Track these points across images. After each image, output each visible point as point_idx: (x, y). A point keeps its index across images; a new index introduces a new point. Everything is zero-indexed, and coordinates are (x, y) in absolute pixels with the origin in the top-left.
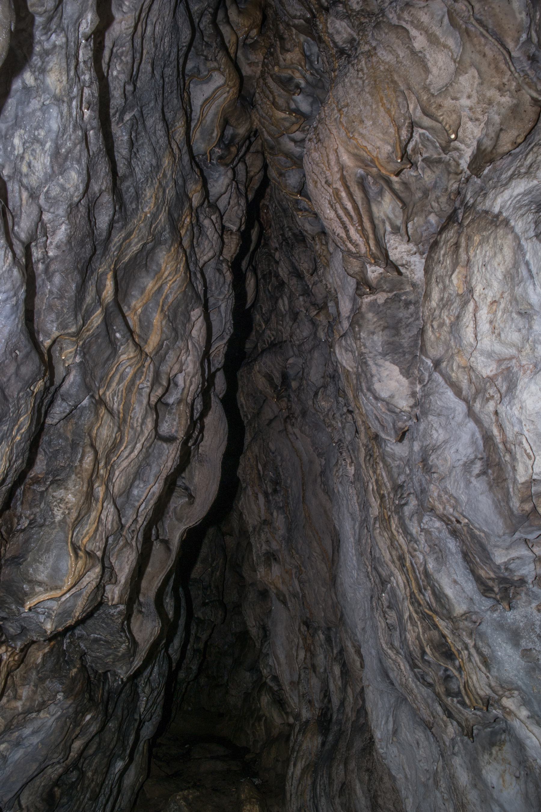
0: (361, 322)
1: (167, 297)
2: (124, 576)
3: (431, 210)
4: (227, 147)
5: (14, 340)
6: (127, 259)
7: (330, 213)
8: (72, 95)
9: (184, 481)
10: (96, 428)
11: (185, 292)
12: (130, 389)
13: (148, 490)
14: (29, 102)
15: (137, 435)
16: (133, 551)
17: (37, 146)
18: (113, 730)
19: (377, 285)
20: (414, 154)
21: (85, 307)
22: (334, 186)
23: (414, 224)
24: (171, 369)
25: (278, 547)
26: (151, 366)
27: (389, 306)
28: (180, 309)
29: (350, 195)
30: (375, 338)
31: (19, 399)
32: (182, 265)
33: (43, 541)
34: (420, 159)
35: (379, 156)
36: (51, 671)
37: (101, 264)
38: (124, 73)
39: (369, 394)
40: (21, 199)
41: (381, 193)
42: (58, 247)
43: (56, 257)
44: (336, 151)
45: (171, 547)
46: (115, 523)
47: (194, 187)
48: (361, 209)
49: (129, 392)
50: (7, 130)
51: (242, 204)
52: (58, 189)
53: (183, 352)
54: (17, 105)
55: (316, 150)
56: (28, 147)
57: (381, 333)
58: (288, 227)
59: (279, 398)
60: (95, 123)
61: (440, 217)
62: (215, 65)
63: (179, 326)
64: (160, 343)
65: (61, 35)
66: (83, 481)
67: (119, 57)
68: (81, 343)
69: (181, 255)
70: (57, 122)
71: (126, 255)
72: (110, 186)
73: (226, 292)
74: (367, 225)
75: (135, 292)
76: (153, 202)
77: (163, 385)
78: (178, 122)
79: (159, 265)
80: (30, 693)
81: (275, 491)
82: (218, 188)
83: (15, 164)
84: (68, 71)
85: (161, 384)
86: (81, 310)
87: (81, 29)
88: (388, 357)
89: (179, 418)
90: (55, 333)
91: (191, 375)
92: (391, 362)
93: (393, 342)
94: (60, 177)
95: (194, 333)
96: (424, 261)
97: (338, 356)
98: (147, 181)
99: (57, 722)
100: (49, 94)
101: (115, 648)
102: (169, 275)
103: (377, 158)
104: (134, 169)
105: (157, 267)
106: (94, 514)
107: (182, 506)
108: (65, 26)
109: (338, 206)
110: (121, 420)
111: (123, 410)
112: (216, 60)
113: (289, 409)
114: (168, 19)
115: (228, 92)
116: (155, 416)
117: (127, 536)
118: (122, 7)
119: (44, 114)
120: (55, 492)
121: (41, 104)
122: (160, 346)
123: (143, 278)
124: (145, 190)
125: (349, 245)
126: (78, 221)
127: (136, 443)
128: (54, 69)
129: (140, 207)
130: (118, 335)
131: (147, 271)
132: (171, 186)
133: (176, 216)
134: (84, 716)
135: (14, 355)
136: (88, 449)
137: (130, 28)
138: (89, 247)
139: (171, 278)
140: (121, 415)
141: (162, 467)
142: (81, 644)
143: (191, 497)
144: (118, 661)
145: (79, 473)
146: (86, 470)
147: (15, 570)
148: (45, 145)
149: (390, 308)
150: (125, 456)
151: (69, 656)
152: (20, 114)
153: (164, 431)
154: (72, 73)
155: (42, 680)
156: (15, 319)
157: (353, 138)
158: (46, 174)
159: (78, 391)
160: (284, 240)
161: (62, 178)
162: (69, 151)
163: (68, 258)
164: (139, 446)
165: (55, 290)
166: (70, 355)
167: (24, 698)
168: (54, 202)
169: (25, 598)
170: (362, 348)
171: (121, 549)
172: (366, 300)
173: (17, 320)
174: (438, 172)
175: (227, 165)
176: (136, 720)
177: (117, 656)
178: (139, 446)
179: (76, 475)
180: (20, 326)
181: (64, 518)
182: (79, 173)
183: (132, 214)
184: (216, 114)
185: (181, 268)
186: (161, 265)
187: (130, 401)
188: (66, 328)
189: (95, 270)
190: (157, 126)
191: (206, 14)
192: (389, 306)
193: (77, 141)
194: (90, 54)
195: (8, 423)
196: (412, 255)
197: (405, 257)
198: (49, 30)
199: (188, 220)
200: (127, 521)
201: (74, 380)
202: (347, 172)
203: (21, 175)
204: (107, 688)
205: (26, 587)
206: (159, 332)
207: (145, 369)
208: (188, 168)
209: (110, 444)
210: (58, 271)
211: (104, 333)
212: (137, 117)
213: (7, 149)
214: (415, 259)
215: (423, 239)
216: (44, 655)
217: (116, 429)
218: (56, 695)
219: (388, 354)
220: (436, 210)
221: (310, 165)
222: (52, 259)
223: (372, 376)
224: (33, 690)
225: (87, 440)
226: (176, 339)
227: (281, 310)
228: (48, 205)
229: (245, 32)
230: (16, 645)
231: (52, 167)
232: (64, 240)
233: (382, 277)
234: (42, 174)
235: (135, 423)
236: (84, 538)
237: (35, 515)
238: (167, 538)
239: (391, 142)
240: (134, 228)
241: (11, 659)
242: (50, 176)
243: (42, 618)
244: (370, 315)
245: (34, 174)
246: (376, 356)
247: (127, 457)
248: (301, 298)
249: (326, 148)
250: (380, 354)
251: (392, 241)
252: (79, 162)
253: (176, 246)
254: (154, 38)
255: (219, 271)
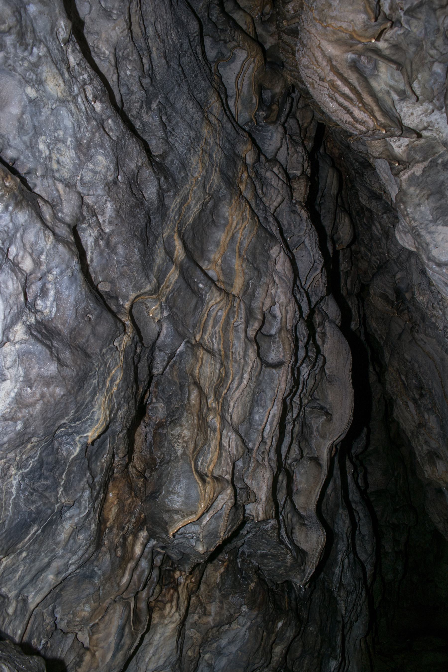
0: (404, 199)
1: (241, 244)
2: (264, 494)
3: (432, 60)
4: (269, 108)
5: (83, 306)
6: (191, 220)
7: (333, 106)
8: (74, 94)
9: (318, 402)
10: (197, 368)
11: (257, 234)
12: (226, 328)
13: (267, 413)
14: (40, 112)
15: (241, 366)
16: (266, 470)
17: (60, 145)
18: (315, 633)
19: (408, 158)
20: (394, 12)
21: (156, 267)
22: (328, 79)
23: (419, 81)
24: (263, 304)
25: (437, 445)
26: (242, 305)
27: (427, 174)
28: (258, 251)
29: (346, 81)
30: (422, 208)
31: (103, 356)
32: (247, 213)
33: (172, 475)
34: (402, 14)
35: (356, 29)
36: (232, 588)
37: (163, 229)
38: (136, 69)
39: (431, 263)
40: (58, 191)
41: (376, 67)
42: (110, 223)
43: (113, 231)
44: (319, 47)
45: (321, 463)
46: (239, 448)
47: (245, 148)
48: (358, 88)
49: (225, 332)
50: (31, 141)
51: (301, 151)
52: (90, 174)
53: (270, 286)
54: (31, 117)
55: (303, 56)
56: (52, 148)
57: (426, 202)
58: (354, 159)
59: (400, 312)
60: (109, 112)
61: (444, 63)
62: (235, 43)
63: (261, 265)
64: (245, 283)
65: (42, 47)
66: (193, 415)
67: (125, 58)
68: (164, 299)
69: (244, 204)
70: (70, 120)
71: (189, 217)
72: (146, 161)
73: (305, 228)
74: (368, 99)
75: (211, 247)
76: (201, 166)
77: (258, 319)
78: (211, 98)
79: (225, 218)
80: (218, 609)
81: (422, 395)
82: (274, 145)
83: (46, 164)
84: (62, 75)
85: (256, 319)
86: (152, 270)
87: (61, 38)
88: (439, 222)
89: (283, 344)
90: (133, 295)
91: (285, 304)
92: (443, 225)
93: (440, 206)
94: (89, 163)
95: (279, 267)
96: (445, 115)
97: (400, 242)
98: (190, 151)
99: (249, 632)
100: (53, 99)
101: (282, 560)
102: (237, 224)
103: (354, 31)
104: (173, 145)
105: (224, 220)
106: (214, 443)
107: (322, 424)
108: (42, 38)
109: (337, 95)
110: (223, 358)
111: (224, 348)
112: (234, 40)
113: (410, 319)
114: (168, 17)
115: (254, 62)
116: (256, 347)
117: (257, 458)
118: (111, 17)
119: (57, 117)
120: (173, 430)
121: (50, 110)
122: (246, 286)
123: (214, 233)
124: (190, 159)
125: (359, 126)
126: (121, 196)
127: (242, 374)
128: (48, 78)
129: (189, 174)
130: (201, 286)
131: (217, 226)
132: (216, 151)
133: (230, 174)
134: (274, 624)
135: (86, 318)
136: (192, 387)
137: (124, 30)
138: (141, 216)
139: (239, 226)
140: (222, 353)
141: (276, 391)
142: (253, 561)
143: (328, 414)
144: (290, 571)
145: (188, 410)
146: (194, 405)
147: (153, 504)
148: (66, 142)
149: (429, 176)
150: (235, 388)
151: (246, 573)
152: (36, 124)
153: (272, 359)
154: (67, 76)
155: (225, 596)
156: (76, 288)
157: (329, 25)
158: (74, 164)
159: (172, 339)
160: (356, 173)
161: (91, 163)
162: (90, 140)
163: (123, 229)
164: (246, 376)
165: (121, 259)
166: (156, 311)
167: (213, 614)
168: (91, 185)
169: (167, 526)
170: (413, 222)
171: (254, 470)
172: (404, 177)
173: (79, 288)
174: (423, 17)
175: (274, 122)
176: (339, 622)
177: (287, 566)
178: (246, 376)
179: (187, 412)
180: (84, 293)
181: (184, 450)
182: (106, 156)
183: (182, 181)
184: (250, 84)
185: (247, 216)
186: (227, 218)
187: (228, 339)
188: (141, 289)
189: (159, 235)
190: (188, 106)
191: (214, 8)
192: (427, 174)
193: (94, 130)
194: (80, 56)
195: (97, 376)
196: (430, 114)
197: (425, 119)
198: (27, 45)
199: (245, 175)
200: (254, 444)
201: (167, 331)
202: (336, 61)
203: (53, 171)
204: (293, 596)
205: (166, 517)
206: (241, 275)
207: (236, 309)
208: (233, 133)
209: (215, 380)
210: (119, 243)
211: (184, 286)
212: (163, 102)
213: (35, 155)
214: (435, 117)
215: (435, 93)
216: (221, 575)
217: (218, 366)
218: (240, 608)
219: (438, 219)
220: (437, 57)
221: (303, 72)
222: (110, 235)
223: (428, 244)
224: (219, 606)
225: (191, 380)
226: (260, 276)
227: (376, 235)
228: (86, 189)
229: (259, 11)
230: (185, 568)
231: (79, 158)
232: (114, 215)
233: (410, 148)
234: (72, 166)
235: (238, 356)
236: (209, 465)
237: (164, 454)
238: (316, 456)
239: (361, 8)
240: (188, 193)
241: (188, 582)
242: (79, 166)
243: (193, 542)
244: (412, 190)
245: (64, 167)
246: (427, 225)
247: (237, 388)
248: (385, 216)
249: (310, 49)
250: (431, 221)
251: (405, 109)
252: (102, 146)
253: (236, 198)
254: (158, 35)
255: (294, 212)
